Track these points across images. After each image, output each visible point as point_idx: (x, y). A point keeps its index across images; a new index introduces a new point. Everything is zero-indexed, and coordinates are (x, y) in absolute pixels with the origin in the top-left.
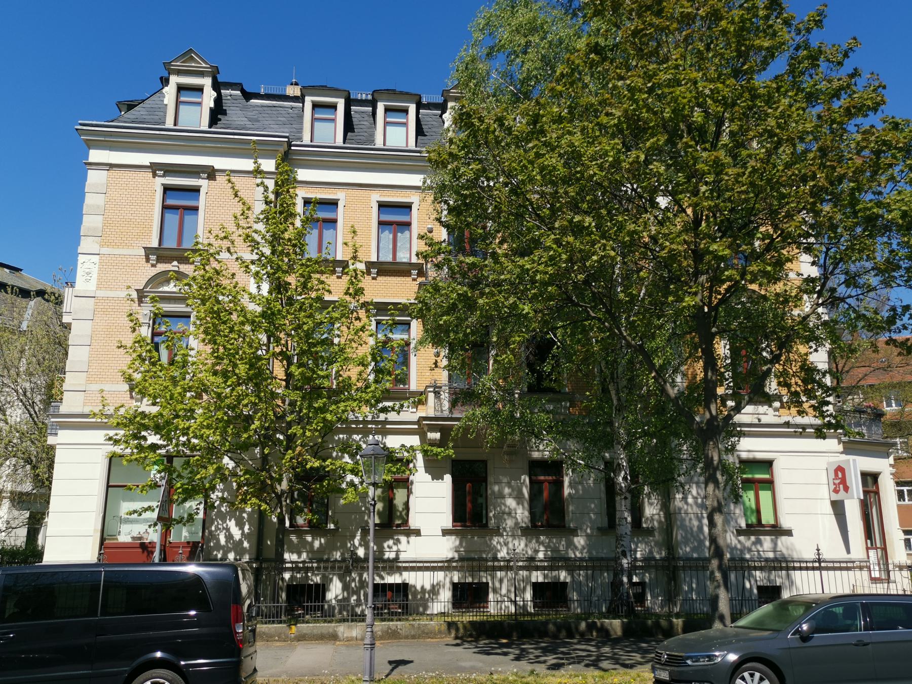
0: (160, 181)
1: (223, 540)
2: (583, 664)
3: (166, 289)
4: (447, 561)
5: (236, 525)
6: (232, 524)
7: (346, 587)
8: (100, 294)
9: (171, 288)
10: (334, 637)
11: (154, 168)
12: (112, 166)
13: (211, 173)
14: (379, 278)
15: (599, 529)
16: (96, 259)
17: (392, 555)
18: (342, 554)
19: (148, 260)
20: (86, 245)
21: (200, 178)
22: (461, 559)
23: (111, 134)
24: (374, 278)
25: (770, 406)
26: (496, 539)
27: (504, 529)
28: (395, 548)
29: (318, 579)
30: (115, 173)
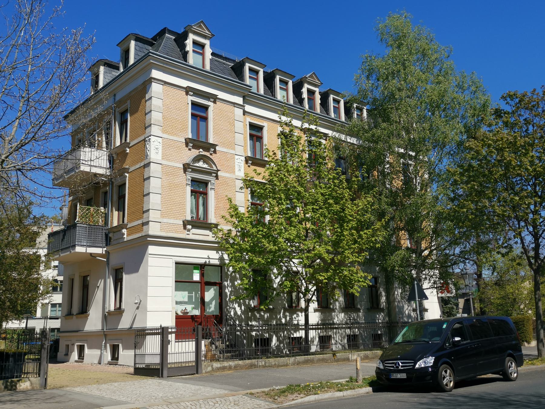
0: (191, 98)
1: (232, 313)
2: (542, 348)
3: (197, 165)
4: (315, 325)
5: (238, 306)
6: (236, 306)
7: (278, 340)
8: (163, 162)
9: (201, 164)
10: (348, 359)
11: (188, 90)
12: (166, 83)
13: (214, 99)
14: (192, 150)
15: (368, 309)
16: (160, 140)
17: (296, 322)
18: (276, 322)
19: (187, 145)
20: (154, 130)
21: (209, 101)
22: (323, 324)
23: (167, 63)
24: (190, 150)
25: (211, 231)
26: (333, 314)
27: (336, 309)
28: (297, 319)
29: (267, 335)
30: (167, 88)
